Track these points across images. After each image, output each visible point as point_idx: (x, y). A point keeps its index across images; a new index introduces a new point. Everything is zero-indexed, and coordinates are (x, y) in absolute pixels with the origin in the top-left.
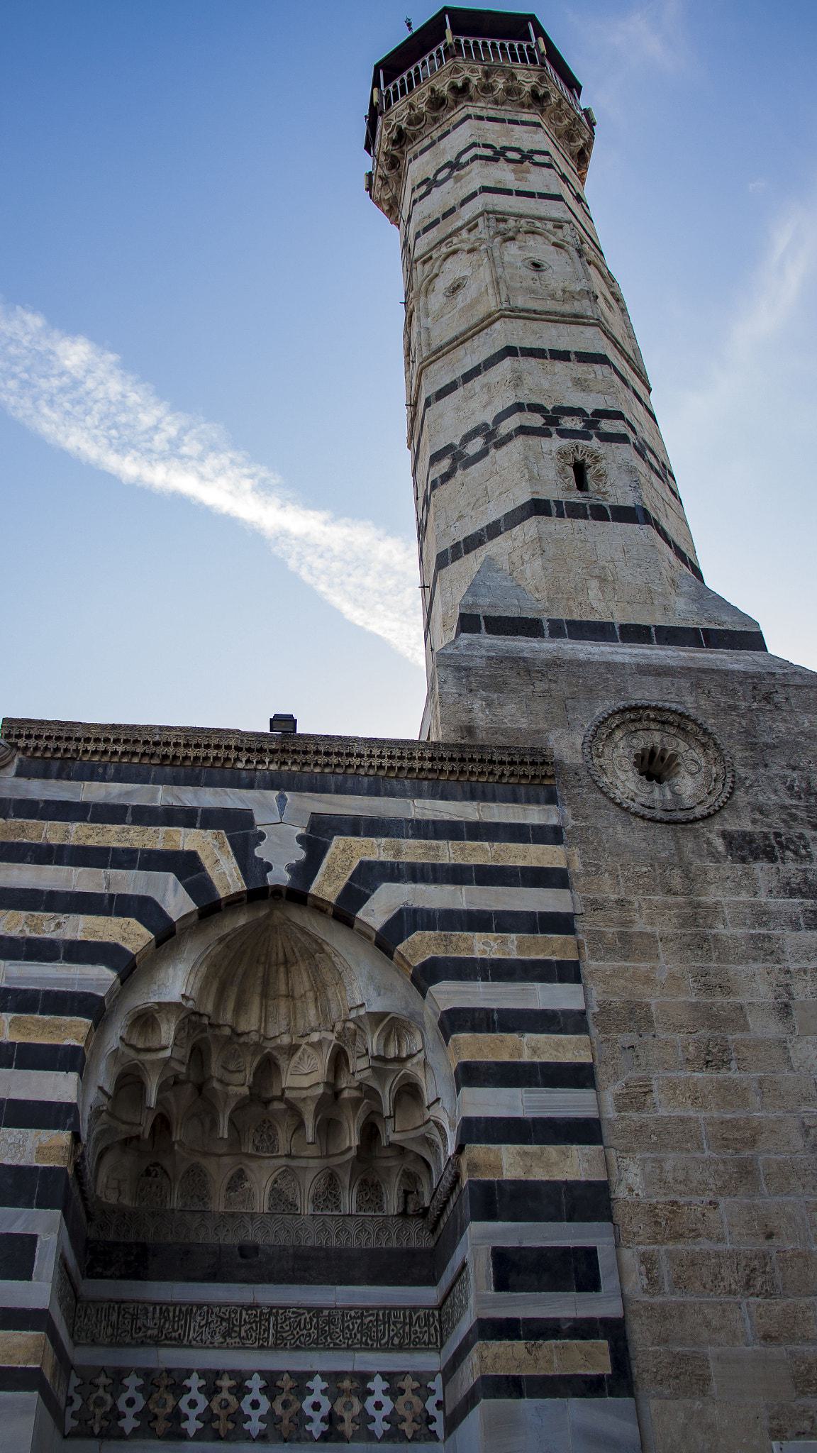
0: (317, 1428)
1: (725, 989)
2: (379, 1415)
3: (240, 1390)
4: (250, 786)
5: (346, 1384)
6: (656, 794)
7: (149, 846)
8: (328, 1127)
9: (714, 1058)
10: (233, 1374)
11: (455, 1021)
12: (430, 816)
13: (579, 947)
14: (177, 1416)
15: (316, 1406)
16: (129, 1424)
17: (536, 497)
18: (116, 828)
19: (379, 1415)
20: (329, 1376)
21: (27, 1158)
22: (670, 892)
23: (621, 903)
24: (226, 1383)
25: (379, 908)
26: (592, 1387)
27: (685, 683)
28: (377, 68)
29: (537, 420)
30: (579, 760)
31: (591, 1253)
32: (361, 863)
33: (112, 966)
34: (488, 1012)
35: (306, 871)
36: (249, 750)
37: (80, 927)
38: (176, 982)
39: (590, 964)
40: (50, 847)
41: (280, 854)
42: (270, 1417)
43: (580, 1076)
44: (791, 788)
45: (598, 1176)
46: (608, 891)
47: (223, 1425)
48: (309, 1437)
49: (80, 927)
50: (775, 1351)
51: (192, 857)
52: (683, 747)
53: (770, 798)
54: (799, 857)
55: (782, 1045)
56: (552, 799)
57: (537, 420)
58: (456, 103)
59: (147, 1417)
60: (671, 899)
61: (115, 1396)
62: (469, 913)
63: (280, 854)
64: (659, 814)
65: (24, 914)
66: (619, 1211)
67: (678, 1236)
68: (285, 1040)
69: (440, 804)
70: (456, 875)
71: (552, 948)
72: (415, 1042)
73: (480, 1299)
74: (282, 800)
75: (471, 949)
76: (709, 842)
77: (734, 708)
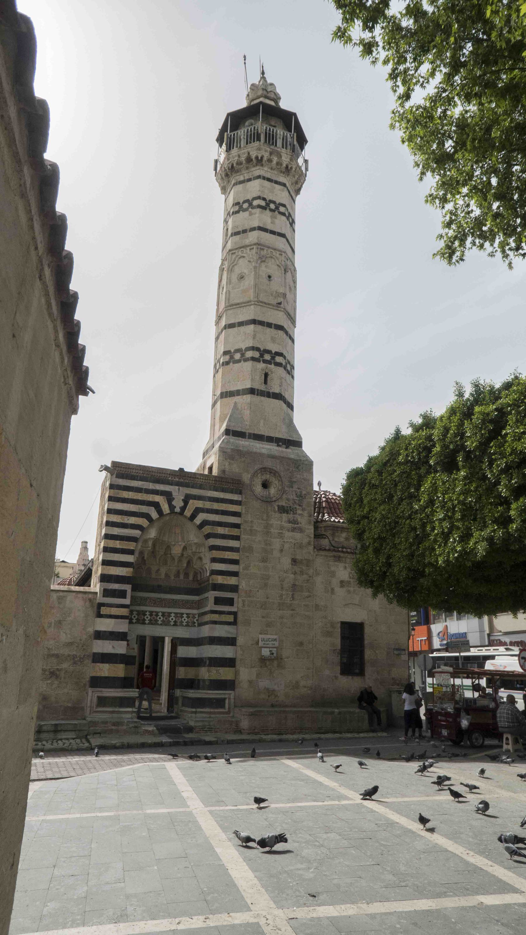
0: (172, 623)
1: (270, 545)
2: (185, 621)
3: (157, 615)
4: (172, 485)
5: (179, 615)
6: (265, 493)
7: (148, 500)
8: (180, 561)
9: (264, 560)
10: (155, 612)
11: (213, 548)
12: (212, 496)
13: (241, 532)
14: (144, 620)
15: (172, 619)
17: (252, 387)
20: (175, 613)
22: (263, 520)
23: (252, 521)
24: (154, 614)
25: (198, 520)
26: (229, 623)
27: (278, 461)
28: (229, 115)
29: (257, 355)
30: (248, 482)
31: (233, 599)
32: (196, 508)
34: (219, 546)
35: (183, 509)
36: (172, 475)
37: (132, 520)
39: (242, 536)
40: (125, 498)
41: (178, 503)
43: (235, 562)
44: (296, 494)
45: (237, 584)
46: (249, 518)
47: (153, 622)
48: (170, 625)
49: (132, 520)
53: (291, 497)
54: (294, 514)
55: (279, 559)
56: (240, 493)
58: (257, 165)
60: (263, 522)
61: (131, 615)
62: (218, 522)
63: (178, 503)
64: (264, 499)
65: (120, 516)
66: (240, 591)
67: (250, 597)
68: (173, 543)
69: (215, 493)
71: (235, 532)
73: (210, 606)
74: (179, 489)
76: (274, 507)
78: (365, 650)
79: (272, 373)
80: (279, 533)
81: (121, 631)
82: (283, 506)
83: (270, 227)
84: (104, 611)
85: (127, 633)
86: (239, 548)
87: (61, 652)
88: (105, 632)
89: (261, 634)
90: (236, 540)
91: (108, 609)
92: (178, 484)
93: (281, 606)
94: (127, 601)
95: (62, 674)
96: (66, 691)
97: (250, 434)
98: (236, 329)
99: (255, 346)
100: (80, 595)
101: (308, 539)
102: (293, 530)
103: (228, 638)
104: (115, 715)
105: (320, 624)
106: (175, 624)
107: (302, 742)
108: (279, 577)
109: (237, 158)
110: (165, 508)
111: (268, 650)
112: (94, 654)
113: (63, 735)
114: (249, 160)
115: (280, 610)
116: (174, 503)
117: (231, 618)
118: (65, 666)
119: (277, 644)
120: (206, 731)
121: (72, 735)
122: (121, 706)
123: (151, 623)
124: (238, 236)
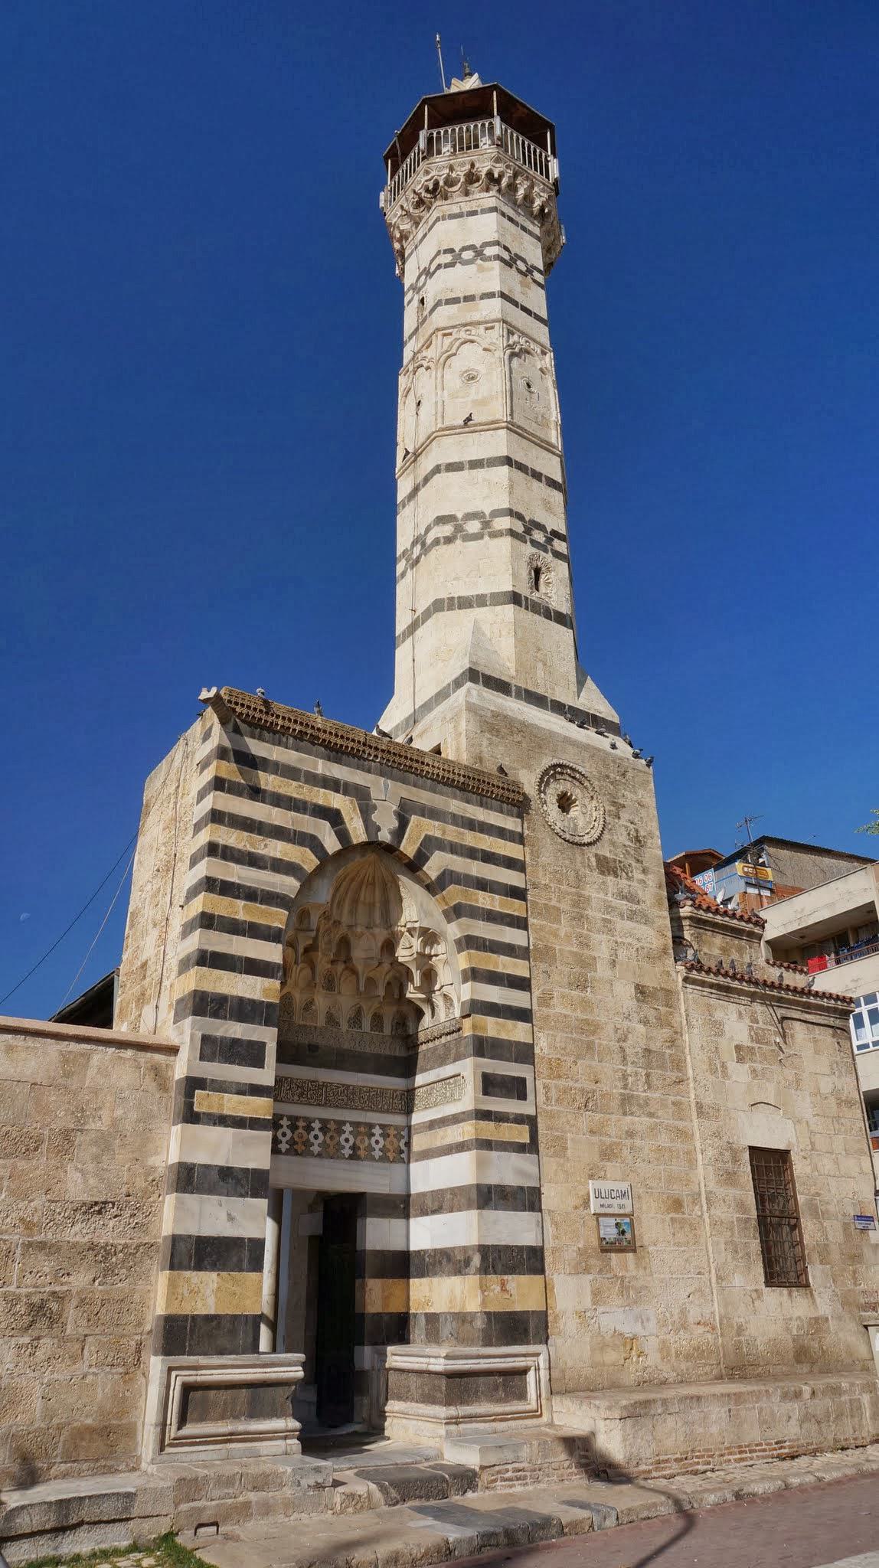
0: (347, 1152)
2: (377, 1147)
3: (309, 1129)
5: (362, 1129)
9: (582, 984)
10: (306, 1119)
15: (347, 1140)
18: (295, 783)
19: (377, 1147)
26: (521, 1148)
31: (523, 1081)
33: (298, 879)
35: (399, 833)
37: (277, 849)
39: (531, 921)
42: (323, 1145)
43: (522, 984)
47: (300, 1148)
48: (343, 1157)
49: (277, 849)
50: (595, 1139)
51: (337, 813)
52: (578, 791)
54: (629, 878)
57: (519, 528)
65: (246, 834)
71: (515, 908)
72: (440, 948)
75: (477, 901)
77: (608, 777)
79: (549, 570)
80: (604, 920)
81: (251, 1165)
82: (605, 858)
83: (518, 298)
84: (203, 1102)
85: (266, 1172)
86: (527, 949)
90: (518, 928)
94: (266, 1076)
97: (519, 689)
98: (465, 473)
99: (515, 509)
101: (662, 941)
102: (632, 916)
106: (354, 1157)
108: (616, 1030)
109: (447, 171)
111: (612, 1221)
114: (471, 178)
116: (374, 817)
117: (522, 1134)
118: (79, 1280)
120: (510, 1480)
124: (456, 306)
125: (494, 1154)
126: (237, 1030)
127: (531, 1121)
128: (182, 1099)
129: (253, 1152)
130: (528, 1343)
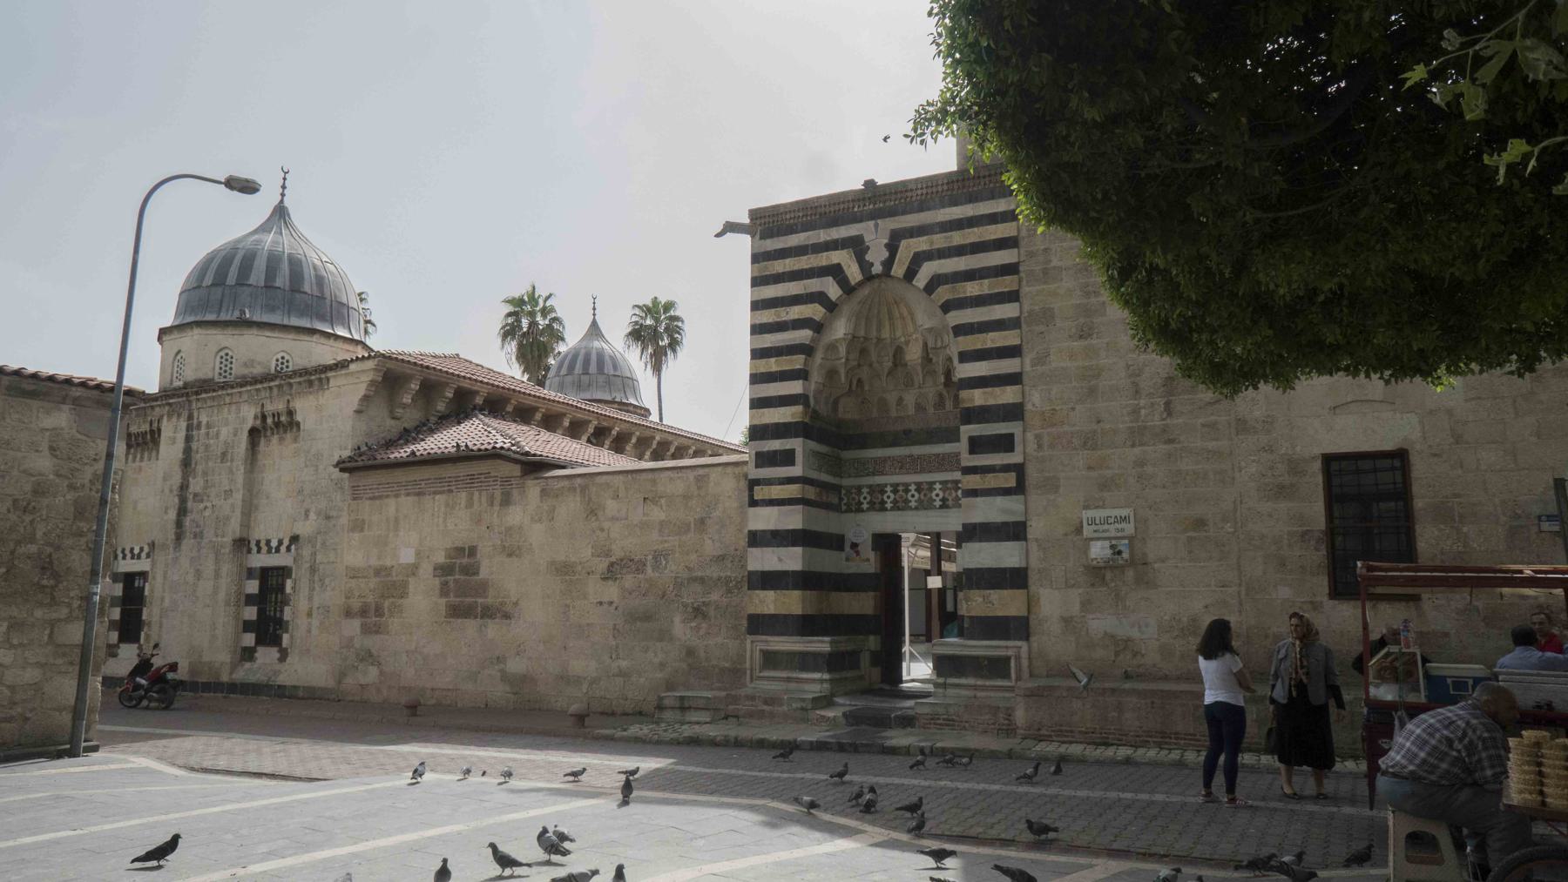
0: (938, 503)
3: (907, 491)
11: (960, 330)
12: (948, 218)
13: (1020, 281)
14: (883, 502)
16: (865, 506)
21: (789, 419)
25: (921, 280)
26: (1006, 492)
31: (1012, 435)
34: (972, 324)
37: (796, 312)
38: (840, 329)
39: (1025, 290)
41: (877, 256)
42: (920, 501)
43: (1013, 352)
49: (796, 312)
50: (1093, 474)
59: (871, 503)
63: (877, 256)
66: (1027, 416)
70: (960, 251)
71: (1006, 284)
74: (876, 226)
78: (1418, 529)
81: (791, 527)
84: (760, 493)
87: (708, 573)
88: (764, 531)
89: (1086, 507)
91: (766, 488)
92: (874, 216)
93: (1137, 435)
94: (796, 470)
95: (712, 613)
96: (720, 640)
100: (729, 470)
103: (1005, 524)
104: (793, 686)
105: (1253, 469)
106: (944, 506)
107: (1058, 771)
108: (1128, 367)
110: (854, 273)
112: (751, 573)
113: (694, 716)
115: (1133, 446)
116: (868, 257)
117: (1010, 480)
118: (715, 596)
119: (1129, 528)
121: (704, 716)
122: (804, 668)
123: (896, 508)
125: (979, 499)
126: (775, 445)
127: (1019, 469)
128: (746, 494)
129: (793, 519)
130: (1008, 639)
